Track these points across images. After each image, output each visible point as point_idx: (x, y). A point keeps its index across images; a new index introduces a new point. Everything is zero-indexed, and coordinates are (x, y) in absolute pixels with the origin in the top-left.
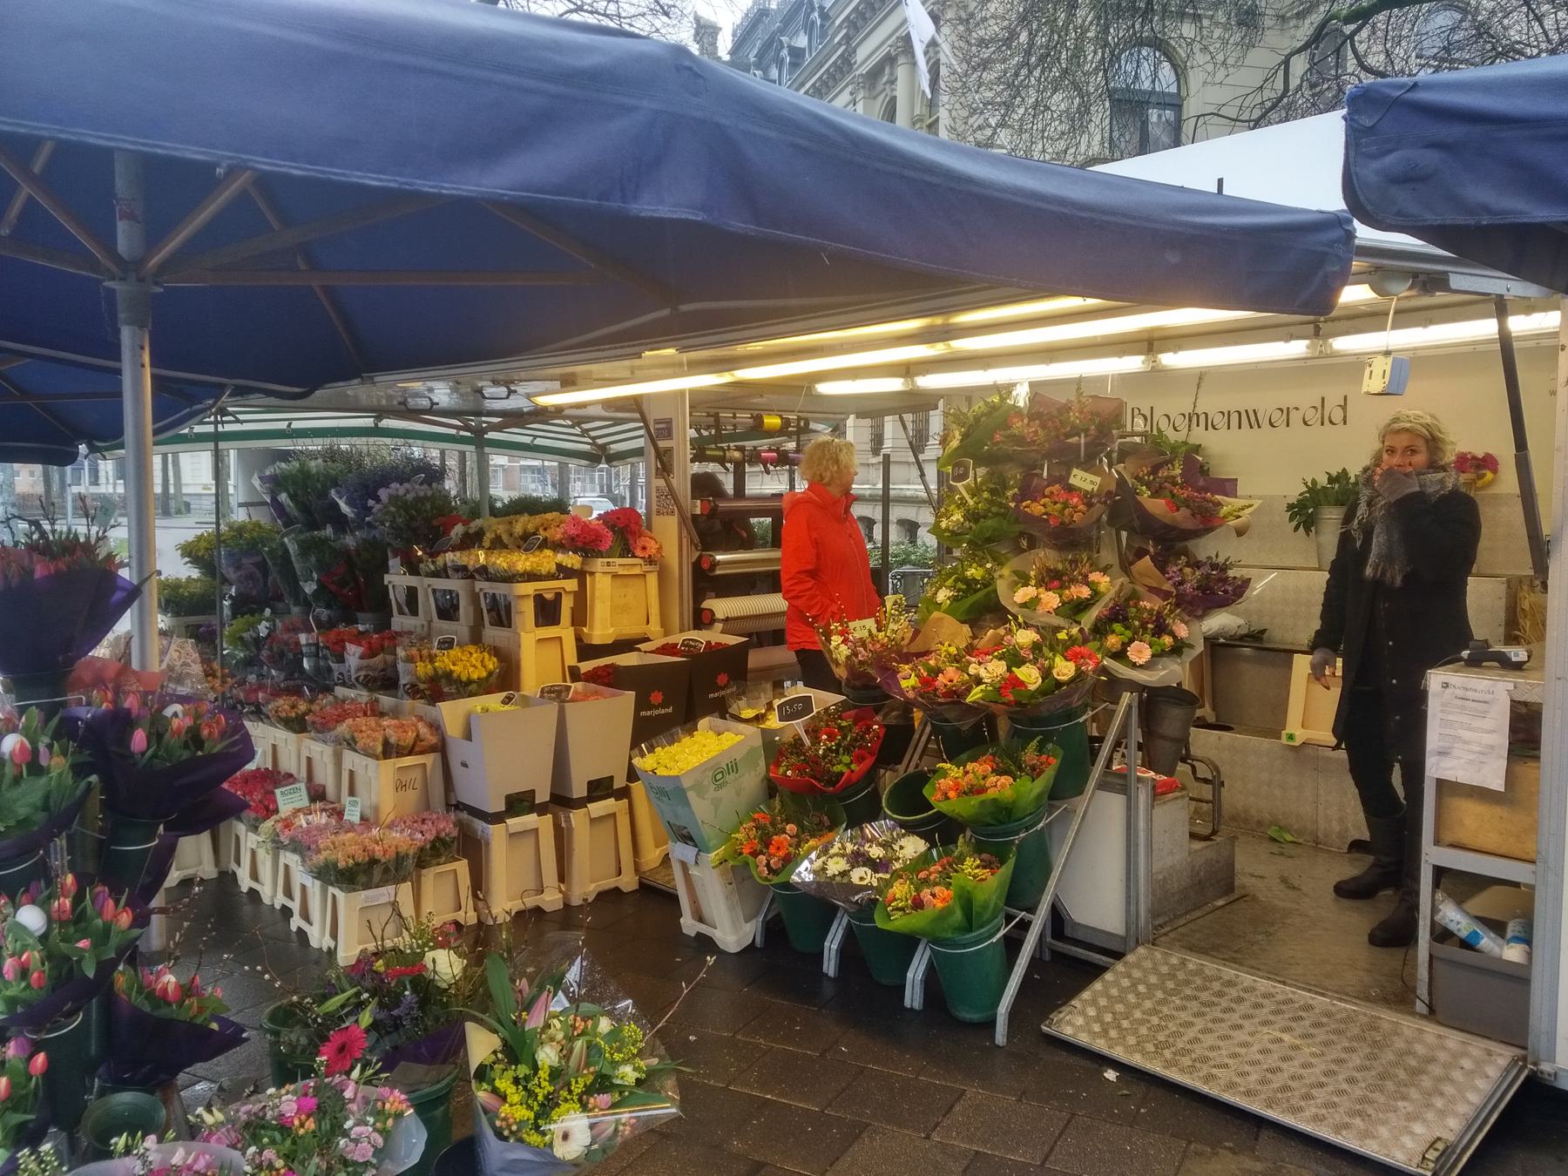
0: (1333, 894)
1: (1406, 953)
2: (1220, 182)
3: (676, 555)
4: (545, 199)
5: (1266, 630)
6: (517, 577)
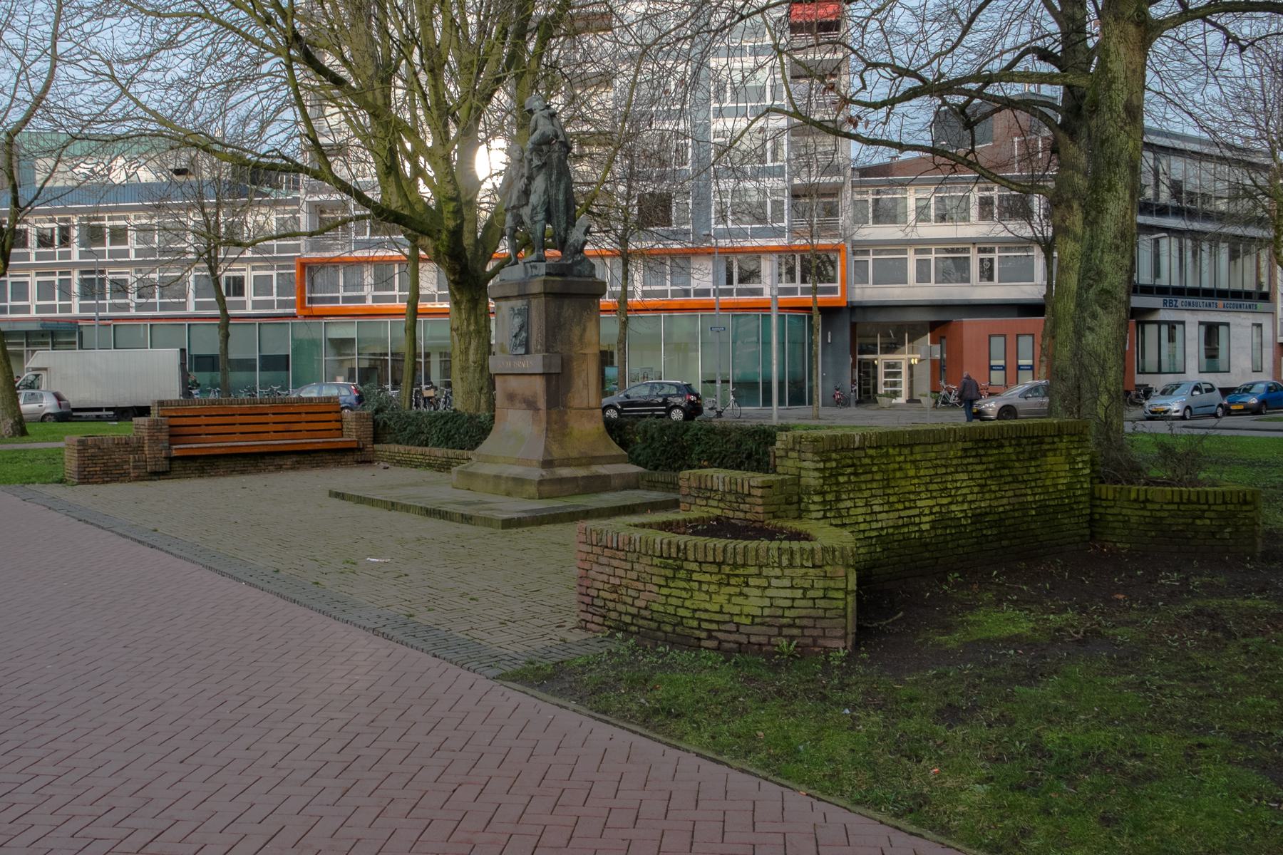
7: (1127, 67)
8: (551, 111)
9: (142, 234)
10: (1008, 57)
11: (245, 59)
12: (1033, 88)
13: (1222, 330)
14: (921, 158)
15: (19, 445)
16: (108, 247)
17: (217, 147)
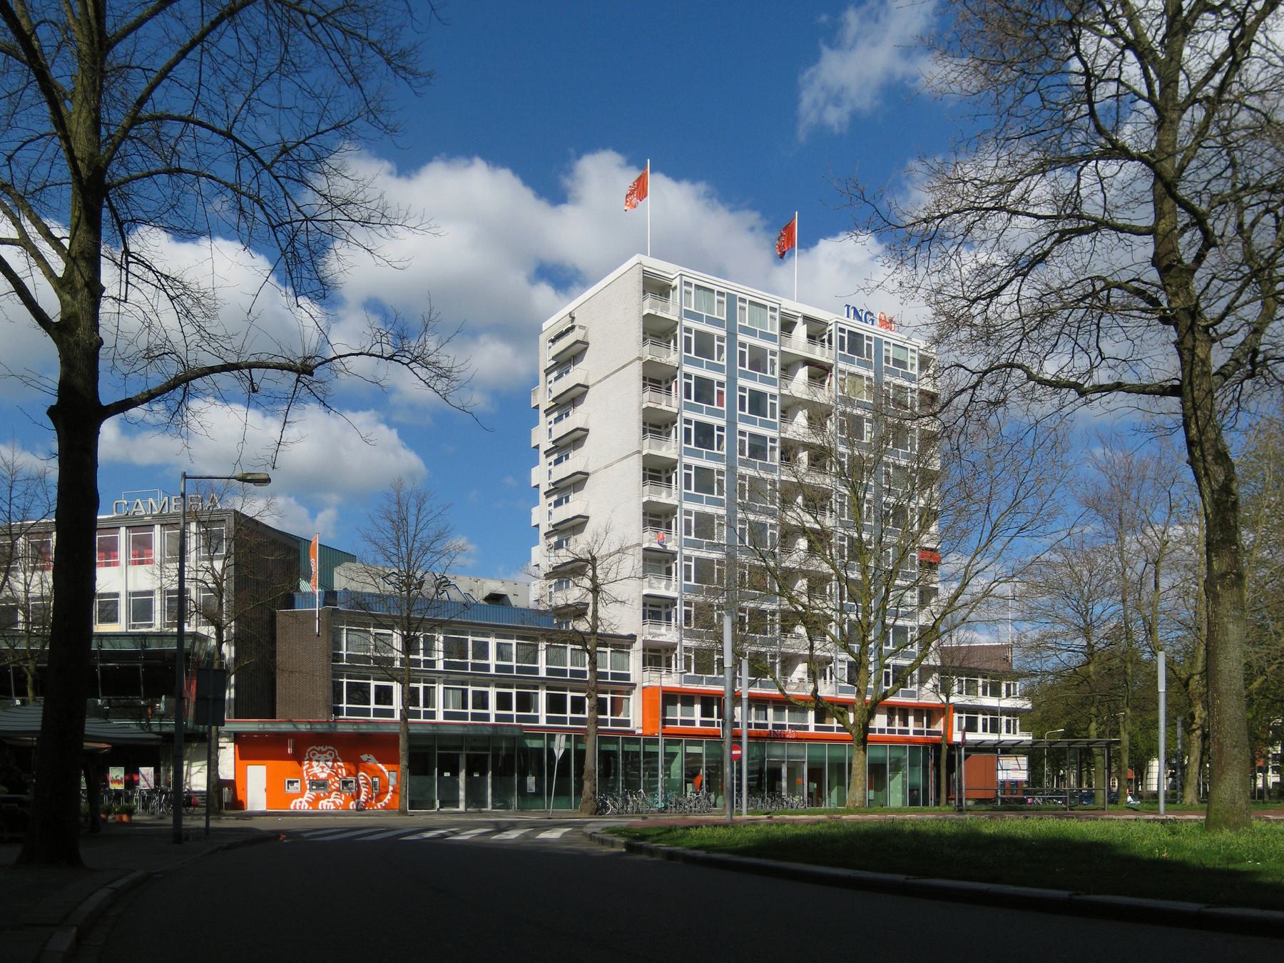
3: (268, 818)
6: (79, 382)
12: (261, 726)
13: (624, 701)
14: (565, 833)
16: (609, 717)
17: (343, 69)
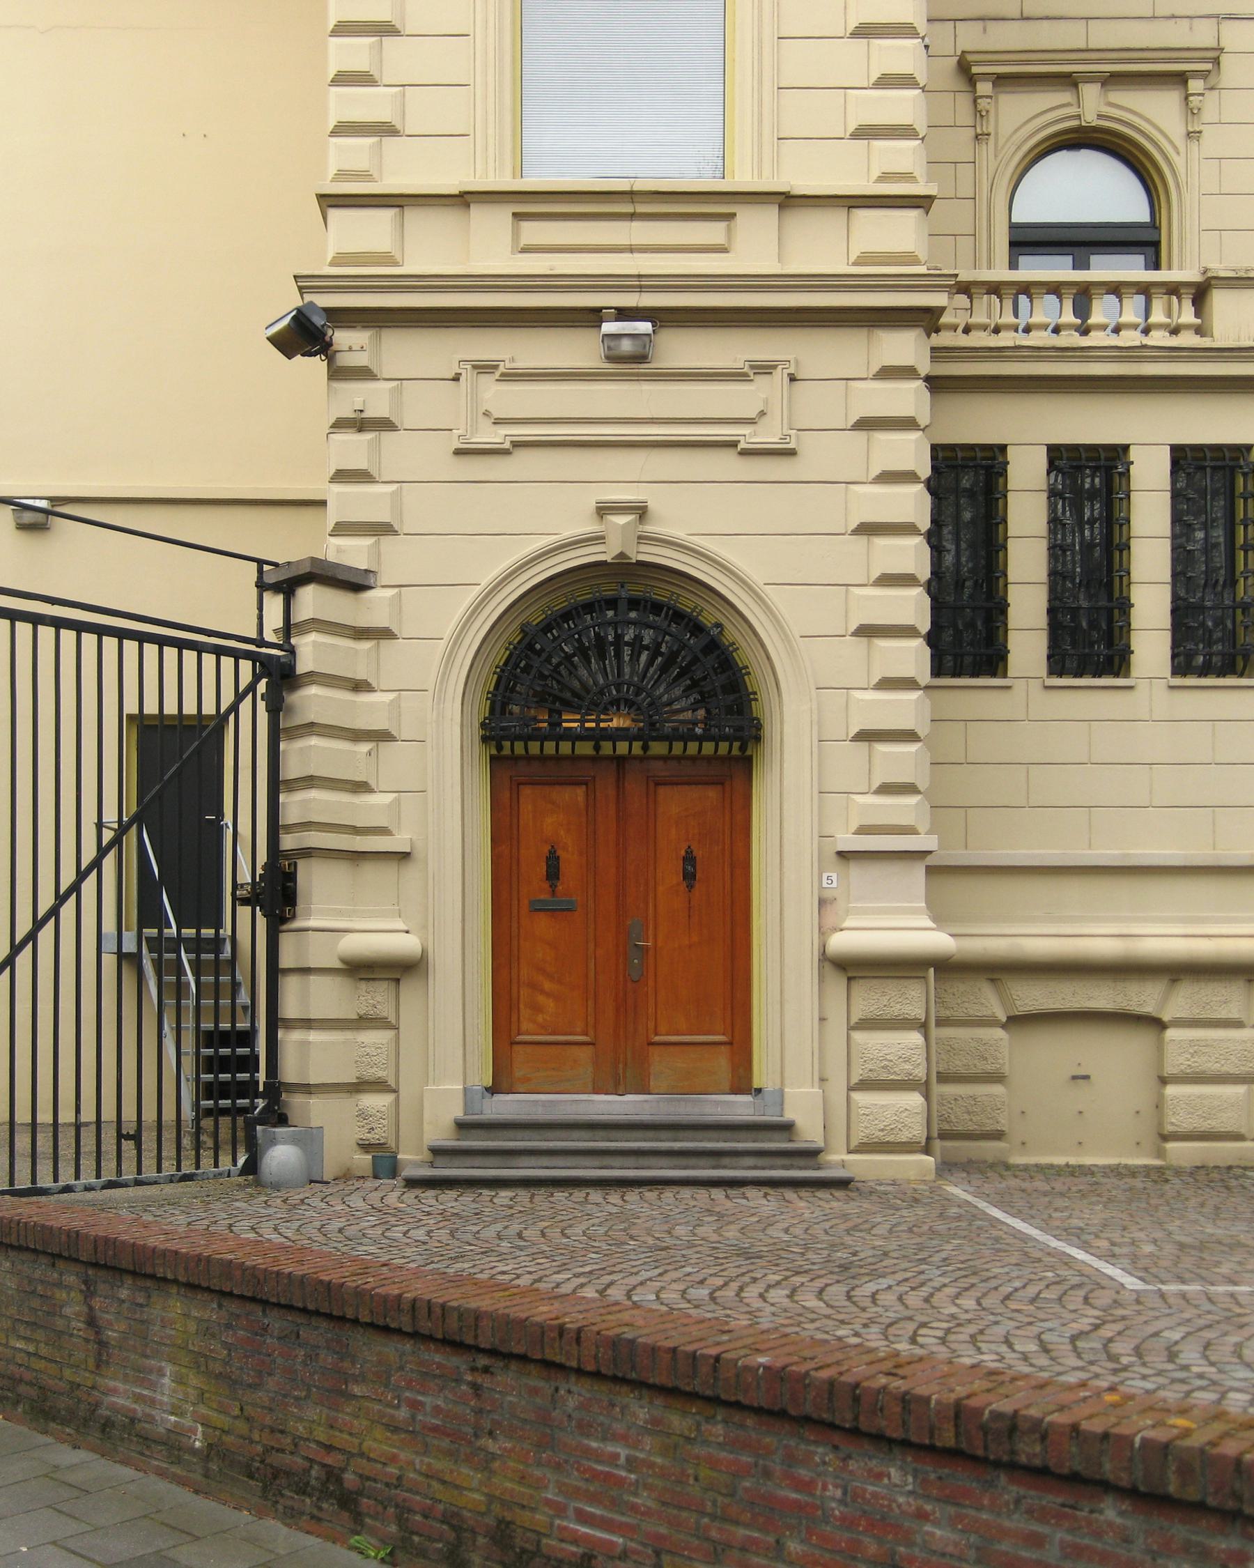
0: (289, 1115)
1: (307, 1089)
2: (985, 30)
4: (594, 1536)
5: (1159, 1077)
7: (906, 1125)
8: (1118, 1297)
9: (952, 1413)
10: (1153, 1379)
11: (1153, 1202)
15: (813, 688)
